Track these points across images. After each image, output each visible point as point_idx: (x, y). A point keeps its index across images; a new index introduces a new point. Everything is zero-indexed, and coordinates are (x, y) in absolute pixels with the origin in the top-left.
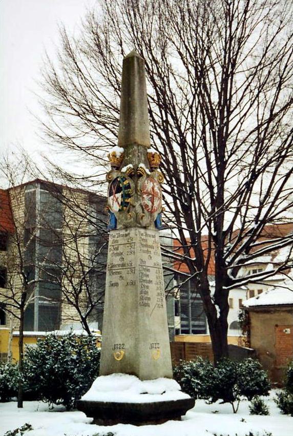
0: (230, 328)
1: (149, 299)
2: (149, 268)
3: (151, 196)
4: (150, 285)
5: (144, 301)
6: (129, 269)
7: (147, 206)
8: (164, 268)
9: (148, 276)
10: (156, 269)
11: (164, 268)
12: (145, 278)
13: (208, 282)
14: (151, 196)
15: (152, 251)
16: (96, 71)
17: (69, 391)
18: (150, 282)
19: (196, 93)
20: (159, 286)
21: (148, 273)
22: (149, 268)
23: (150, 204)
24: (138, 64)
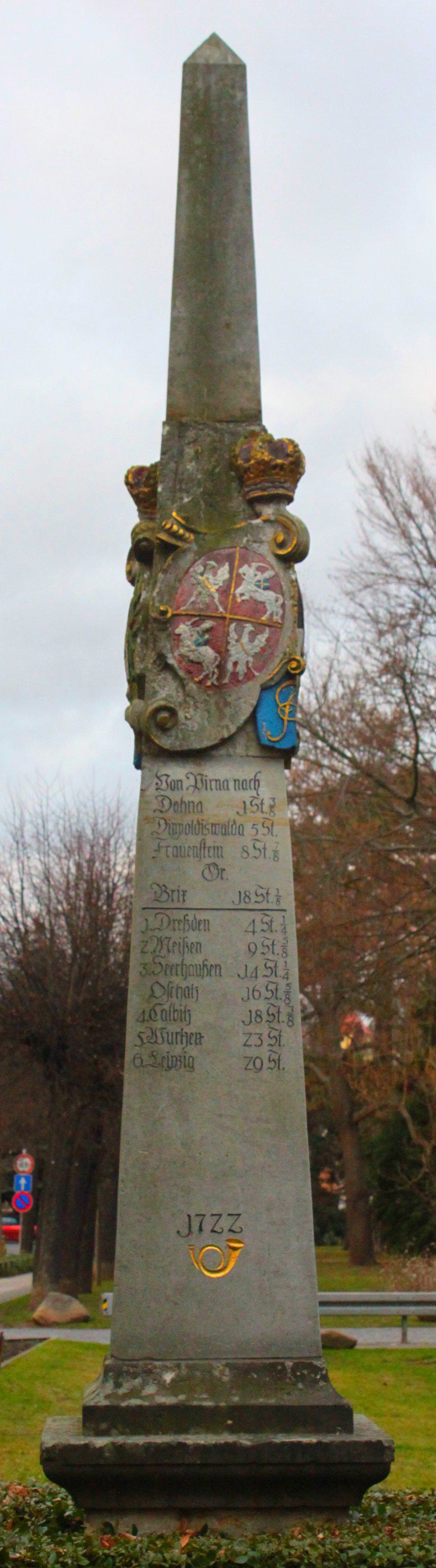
2: (201, 916)
3: (207, 624)
9: (197, 947)
14: (207, 624)
20: (261, 982)
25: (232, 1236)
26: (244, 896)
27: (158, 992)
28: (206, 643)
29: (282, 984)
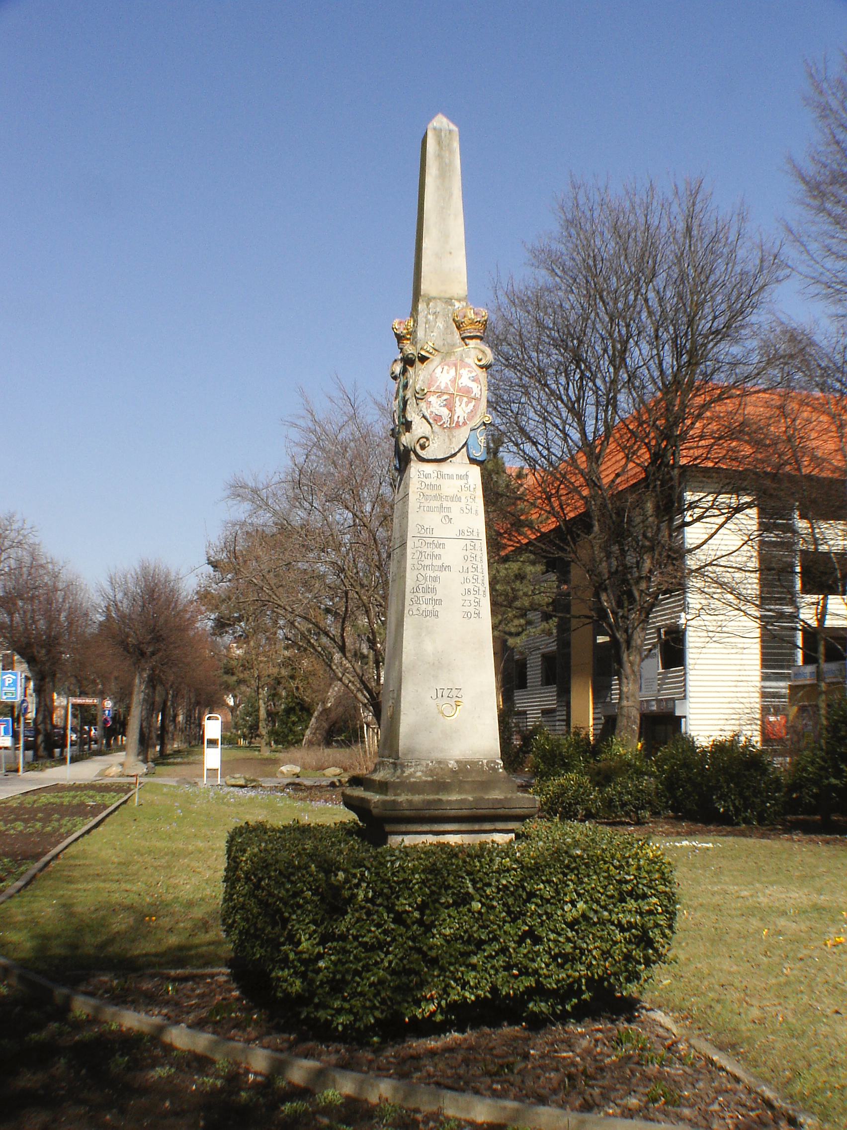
0: (469, 1113)
1: (439, 602)
2: (441, 541)
3: (446, 397)
4: (443, 575)
5: (424, 606)
6: (468, 542)
7: (438, 418)
8: (481, 367)
9: (438, 557)
10: (464, 542)
11: (481, 367)
12: (428, 562)
13: (471, 1123)
14: (446, 397)
15: (455, 507)
16: (719, 554)
17: (407, 1020)
18: (444, 568)
19: (594, 323)
20: (470, 575)
21: (437, 551)
22: (441, 541)
23: (445, 412)
24: (439, 142)
25: (457, 699)
26: (462, 532)
27: (420, 578)
28: (445, 406)
29: (480, 576)
